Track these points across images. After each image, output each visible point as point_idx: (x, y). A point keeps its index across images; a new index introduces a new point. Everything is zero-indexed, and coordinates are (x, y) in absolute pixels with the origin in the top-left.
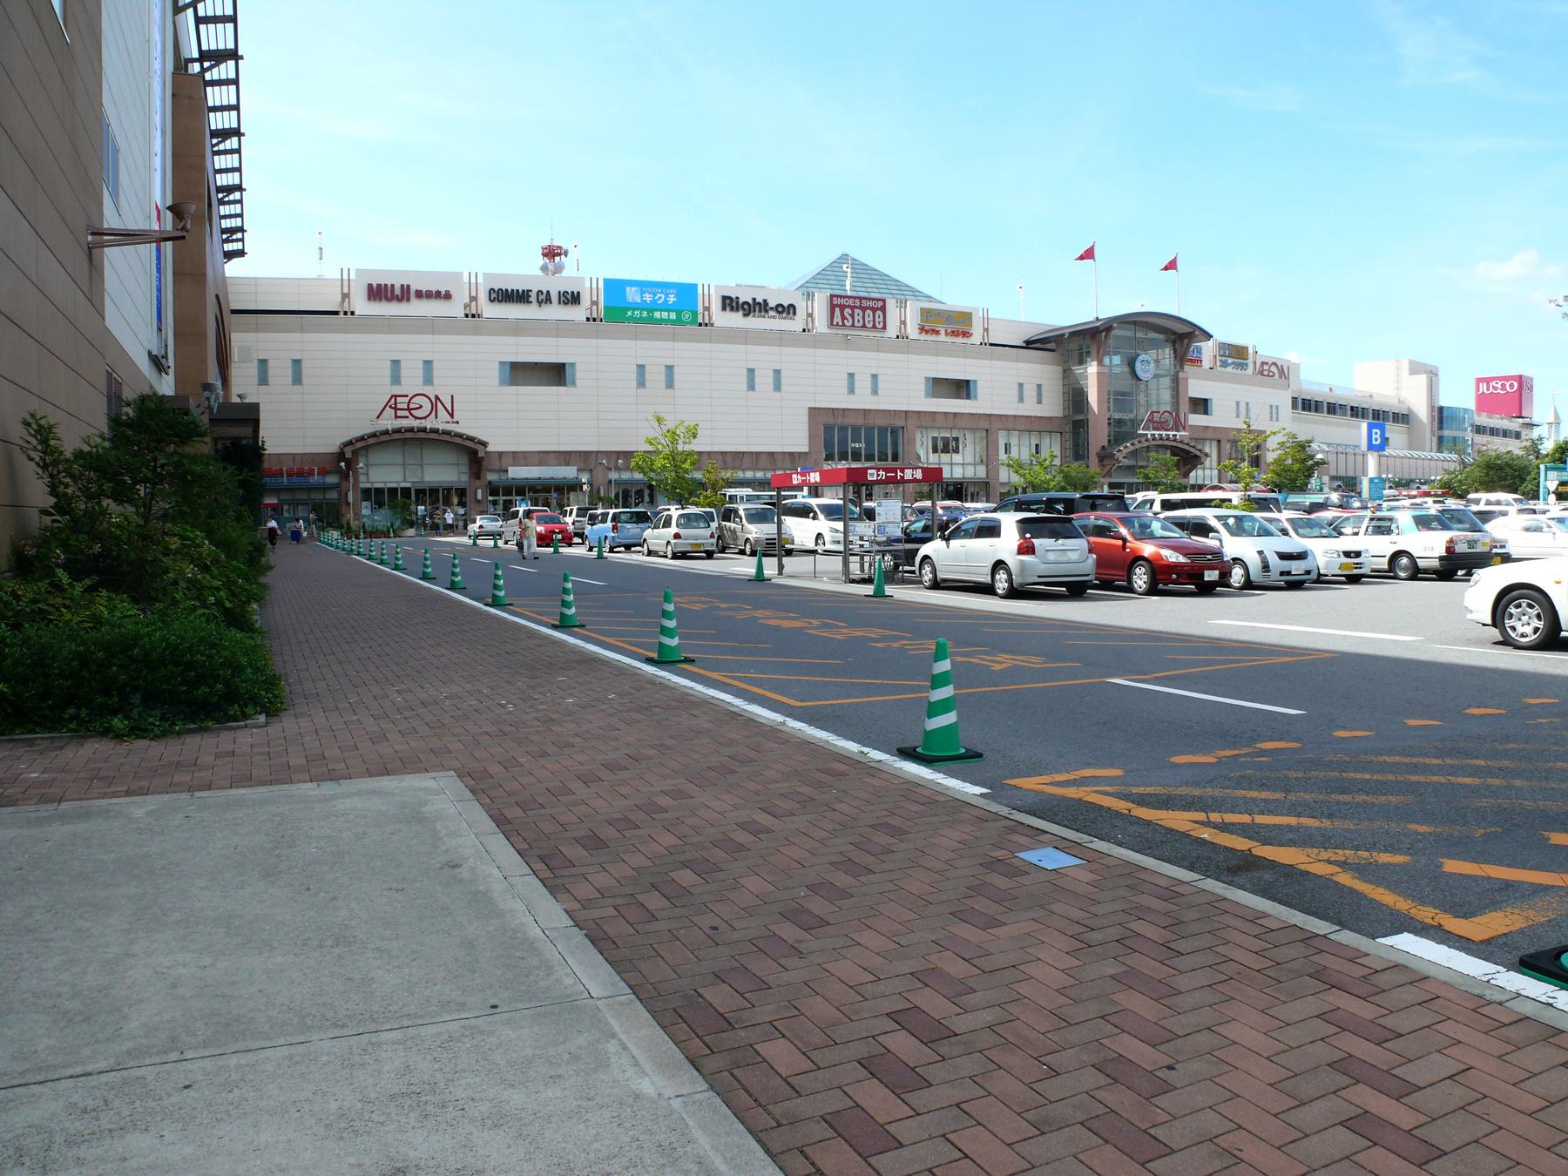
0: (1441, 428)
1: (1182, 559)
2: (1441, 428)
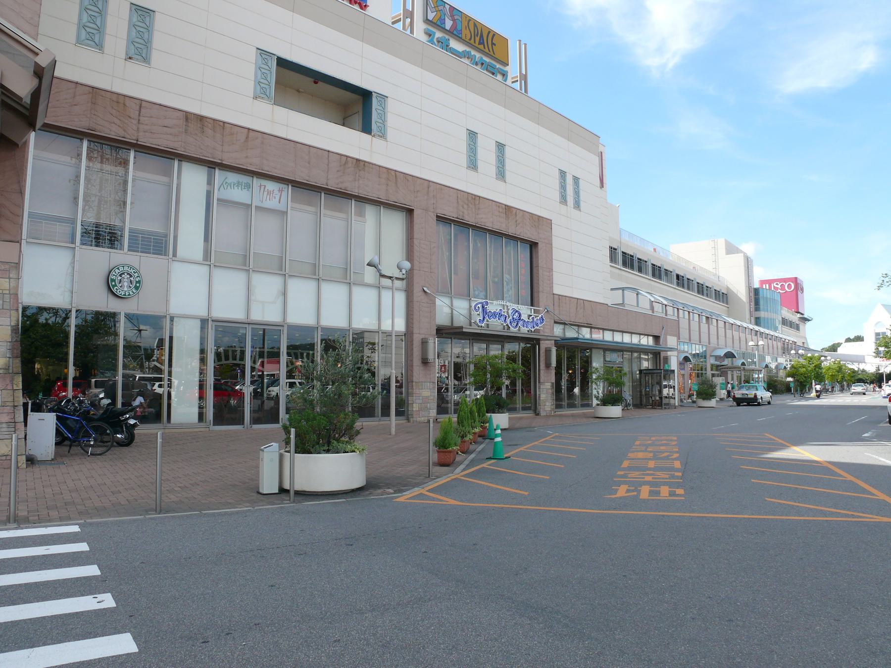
0: (757, 309)
2: (757, 309)
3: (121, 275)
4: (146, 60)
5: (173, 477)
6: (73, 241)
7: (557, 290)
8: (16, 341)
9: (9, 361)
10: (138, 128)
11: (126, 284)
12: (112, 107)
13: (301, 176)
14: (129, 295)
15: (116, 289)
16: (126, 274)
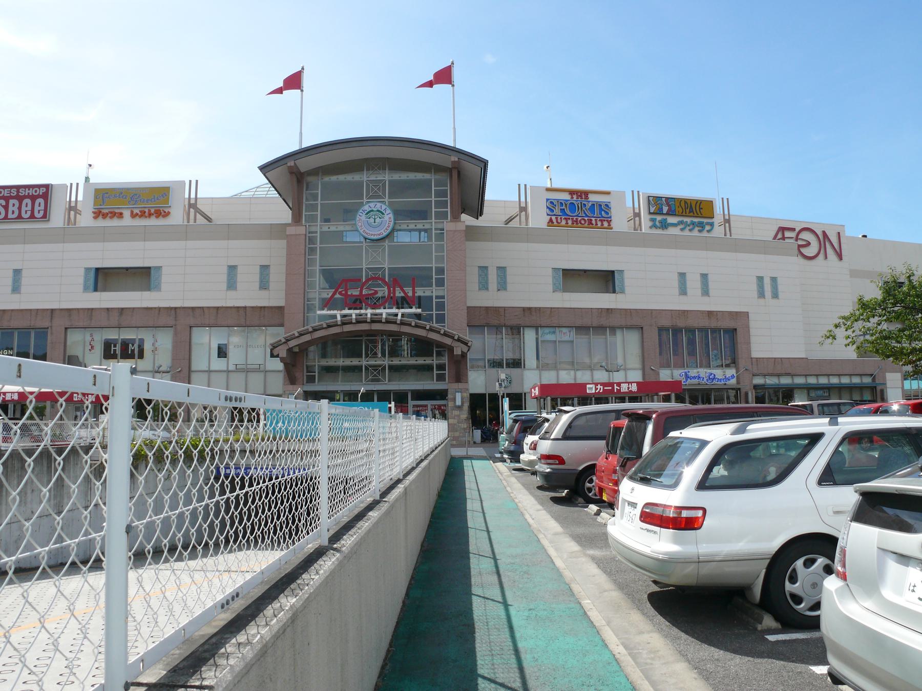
1: (884, 508)
4: (505, 289)
7: (755, 354)
13: (578, 323)
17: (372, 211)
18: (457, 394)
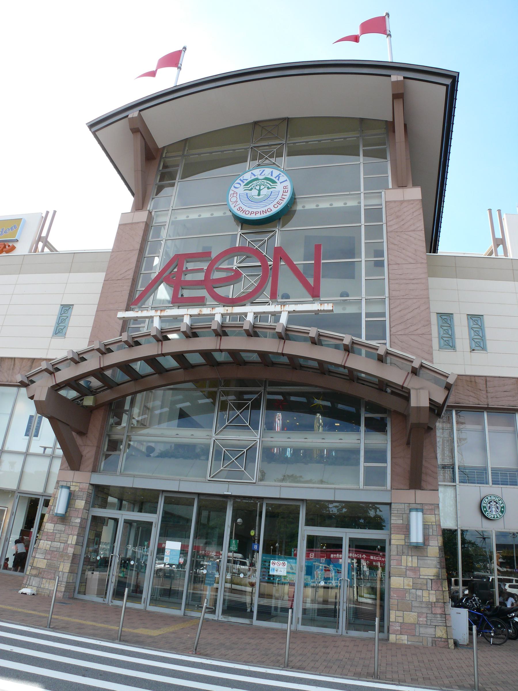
3: (489, 503)
4: (484, 349)
5: (502, 662)
6: (454, 480)
8: (442, 557)
9: (439, 571)
10: (487, 397)
11: (494, 509)
12: (468, 386)
14: (497, 517)
15: (488, 514)
16: (493, 502)
17: (257, 179)
18: (413, 514)
